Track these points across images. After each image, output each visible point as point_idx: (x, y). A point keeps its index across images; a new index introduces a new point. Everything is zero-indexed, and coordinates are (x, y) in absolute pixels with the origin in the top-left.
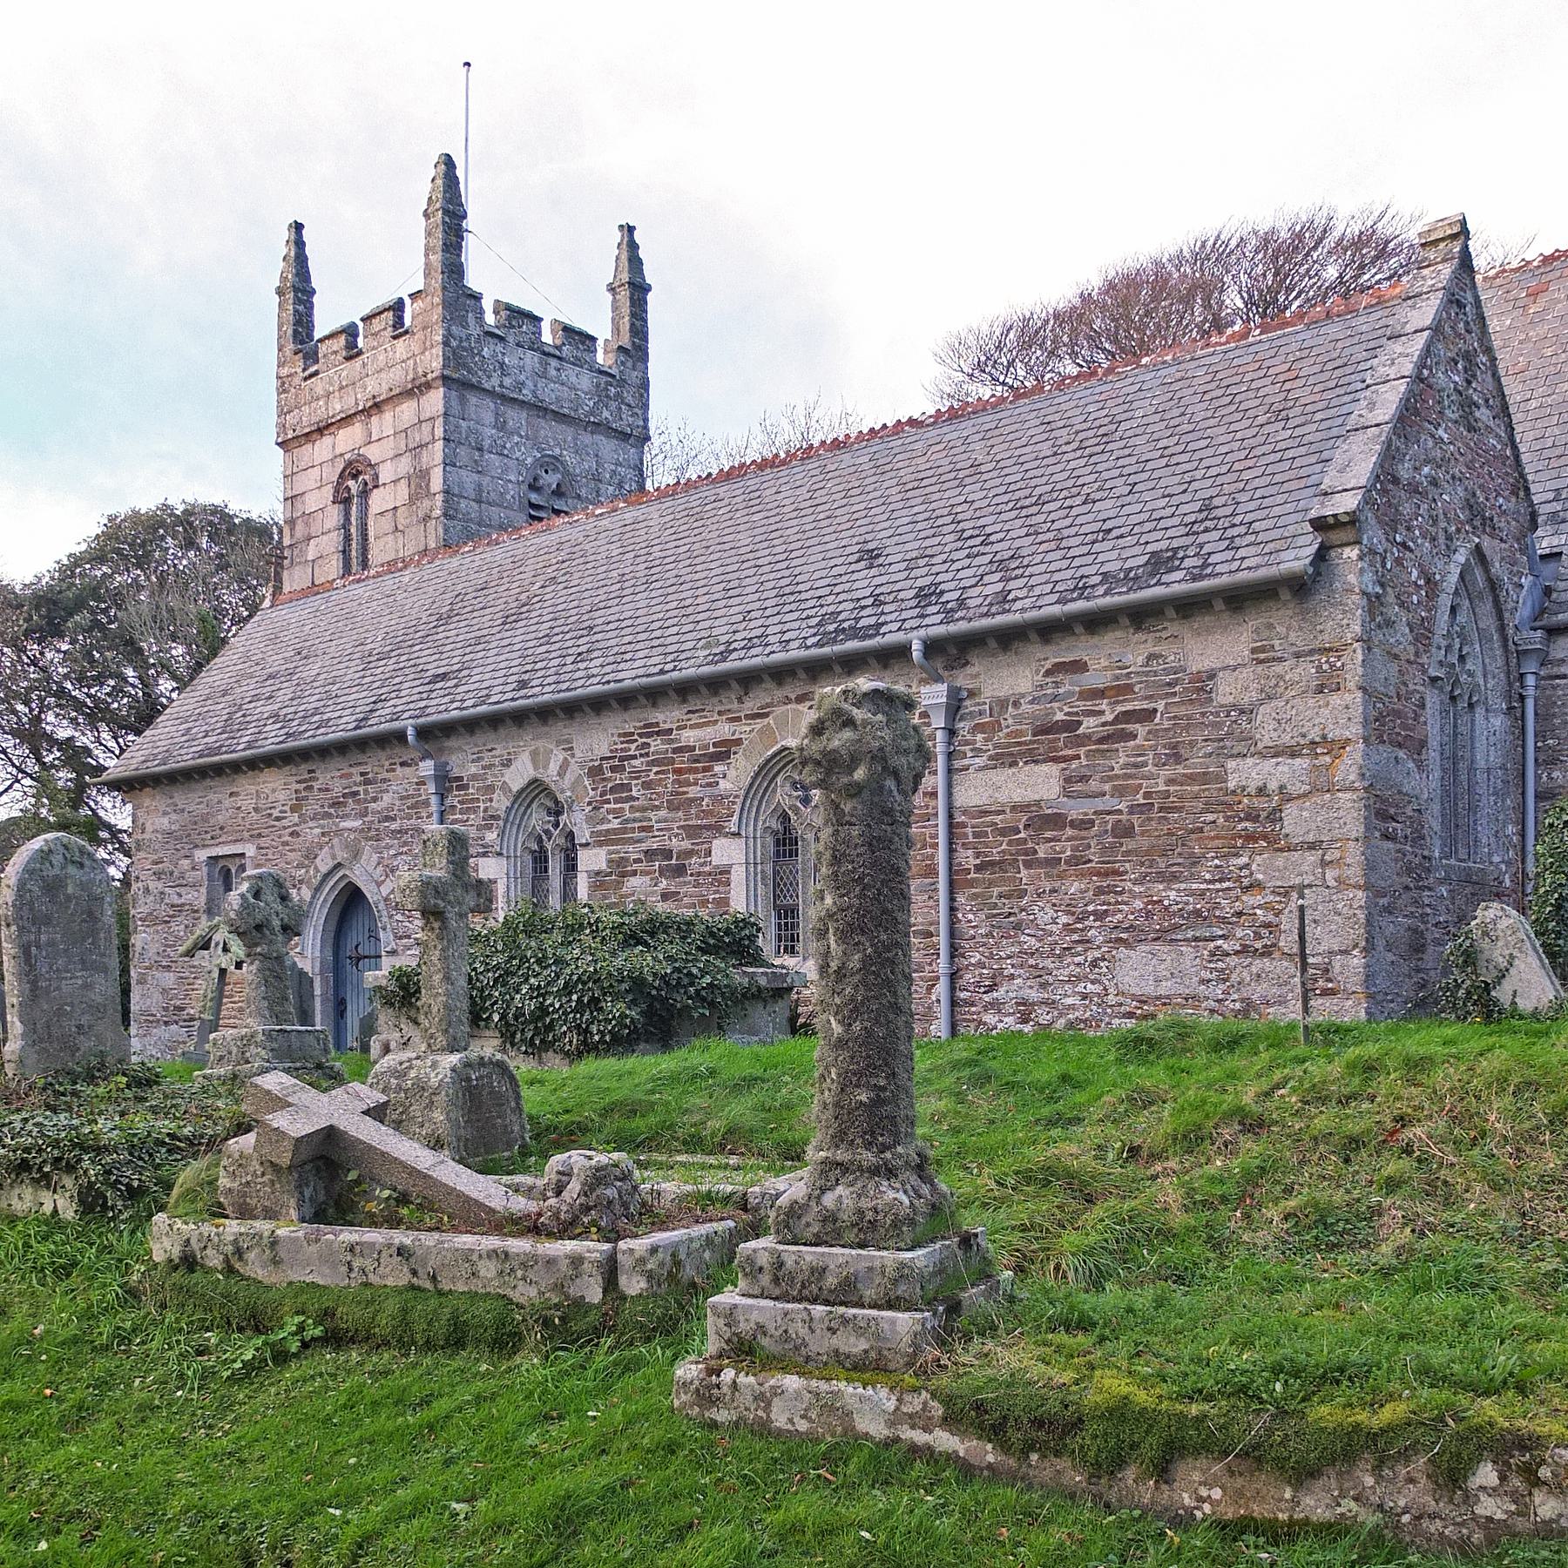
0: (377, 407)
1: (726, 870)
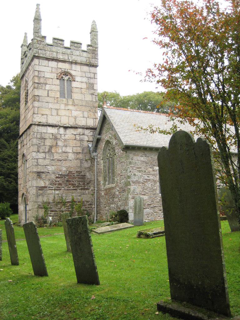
0: (76, 63)
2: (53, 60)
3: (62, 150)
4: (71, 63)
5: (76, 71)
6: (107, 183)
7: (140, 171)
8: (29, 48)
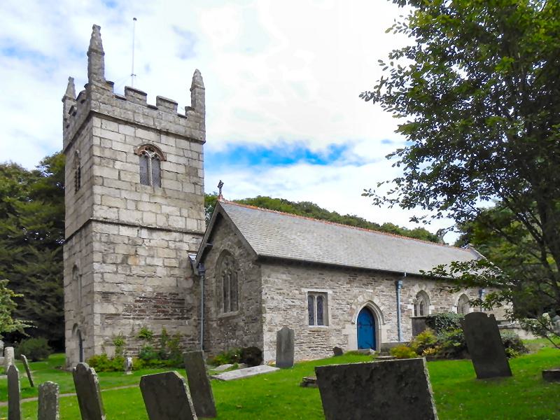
0: (167, 133)
2: (127, 123)
3: (145, 261)
4: (160, 132)
5: (167, 145)
6: (222, 310)
7: (280, 294)
8: (80, 100)
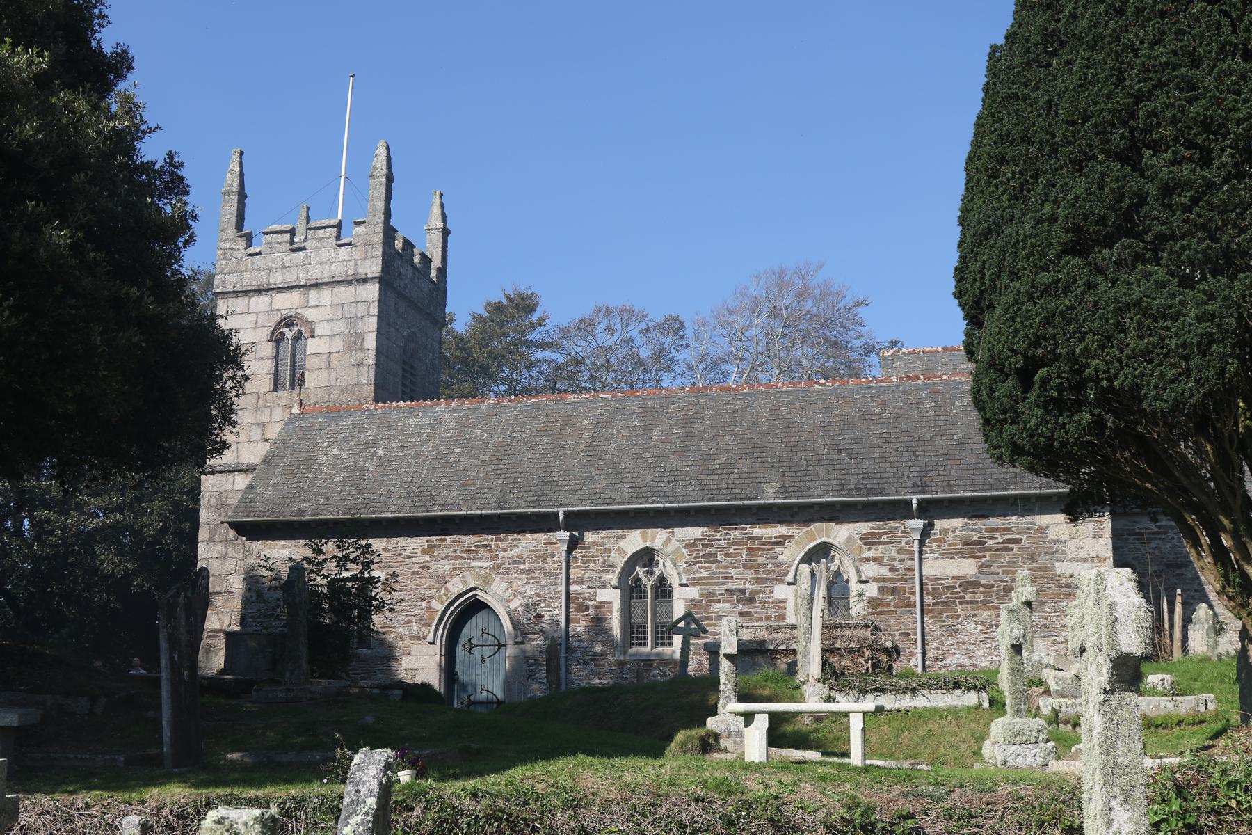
0: (317, 285)
1: (783, 602)
2: (259, 291)
